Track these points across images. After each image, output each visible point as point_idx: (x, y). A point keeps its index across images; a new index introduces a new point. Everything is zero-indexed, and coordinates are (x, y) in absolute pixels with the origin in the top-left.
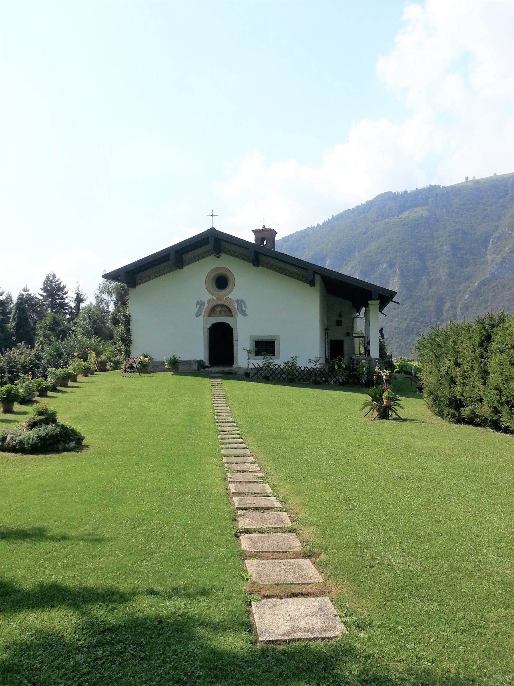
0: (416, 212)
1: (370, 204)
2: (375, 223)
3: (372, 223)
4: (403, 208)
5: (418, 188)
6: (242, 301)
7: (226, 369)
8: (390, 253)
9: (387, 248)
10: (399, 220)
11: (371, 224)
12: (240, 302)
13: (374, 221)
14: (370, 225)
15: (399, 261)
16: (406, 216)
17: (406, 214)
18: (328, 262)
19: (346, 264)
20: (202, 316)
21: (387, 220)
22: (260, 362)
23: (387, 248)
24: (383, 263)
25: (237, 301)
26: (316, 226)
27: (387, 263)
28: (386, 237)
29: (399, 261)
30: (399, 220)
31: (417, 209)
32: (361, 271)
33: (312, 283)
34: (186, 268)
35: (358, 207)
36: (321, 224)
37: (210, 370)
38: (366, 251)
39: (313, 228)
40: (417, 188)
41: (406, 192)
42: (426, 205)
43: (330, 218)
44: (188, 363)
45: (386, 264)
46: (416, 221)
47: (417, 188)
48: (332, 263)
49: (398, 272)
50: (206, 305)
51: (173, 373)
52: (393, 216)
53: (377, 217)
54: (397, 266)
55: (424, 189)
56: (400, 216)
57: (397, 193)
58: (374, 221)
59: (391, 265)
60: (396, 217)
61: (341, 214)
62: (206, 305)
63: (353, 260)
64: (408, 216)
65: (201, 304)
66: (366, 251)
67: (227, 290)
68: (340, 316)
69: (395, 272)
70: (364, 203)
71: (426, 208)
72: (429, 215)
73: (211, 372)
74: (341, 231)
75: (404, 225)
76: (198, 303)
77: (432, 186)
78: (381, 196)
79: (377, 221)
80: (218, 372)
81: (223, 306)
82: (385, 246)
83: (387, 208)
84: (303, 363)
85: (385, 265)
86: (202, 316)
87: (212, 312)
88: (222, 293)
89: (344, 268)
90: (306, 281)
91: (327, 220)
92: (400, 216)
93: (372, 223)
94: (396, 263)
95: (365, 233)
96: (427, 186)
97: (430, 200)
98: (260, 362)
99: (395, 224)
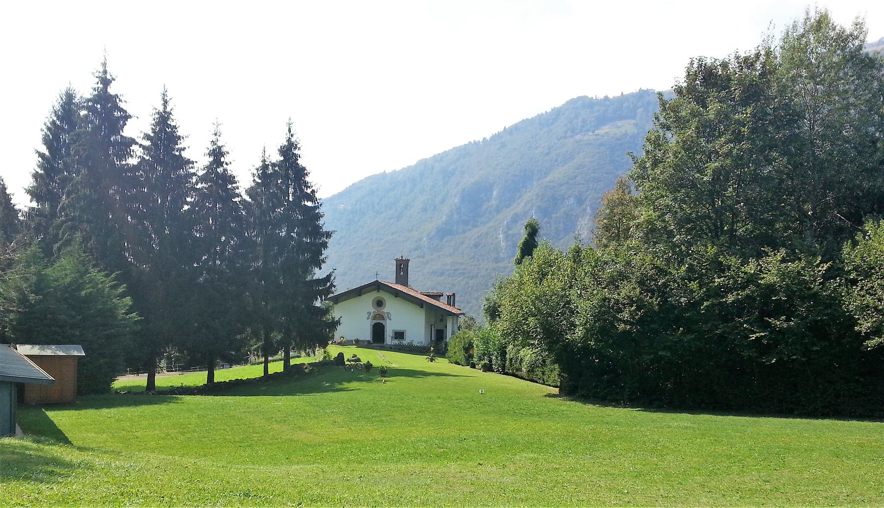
0: (618, 127)
1: (557, 113)
2: (562, 140)
3: (559, 140)
4: (602, 121)
5: (624, 93)
6: (389, 313)
7: (380, 345)
8: (580, 184)
9: (575, 177)
10: (595, 137)
11: (557, 142)
12: (388, 313)
13: (561, 138)
14: (555, 143)
15: (590, 196)
16: (605, 133)
17: (604, 130)
18: (495, 193)
19: (520, 197)
20: (370, 320)
21: (577, 137)
22: (396, 342)
23: (575, 177)
24: (570, 197)
25: (387, 313)
26: (481, 140)
27: (574, 198)
28: (575, 161)
29: (590, 196)
30: (595, 137)
31: (619, 123)
32: (539, 207)
33: (422, 307)
34: (363, 296)
35: (540, 116)
36: (488, 138)
37: (373, 345)
38: (548, 179)
39: (476, 143)
40: (622, 93)
41: (606, 98)
42: (634, 117)
43: (502, 129)
44: (363, 341)
45: (573, 199)
46: (618, 139)
47: (622, 93)
48: (501, 194)
49: (589, 210)
50: (372, 314)
51: (47, 153)
52: (588, 131)
53: (566, 132)
54: (588, 202)
55: (632, 95)
56: (597, 132)
57: (594, 98)
58: (561, 138)
59: (580, 201)
60: (590, 133)
61: (516, 124)
62: (372, 314)
63: (529, 192)
64: (607, 132)
65: (369, 313)
66: (548, 179)
67: (382, 308)
68: (442, 316)
69: (585, 210)
70: (549, 110)
71: (633, 121)
72: (636, 131)
73: (374, 346)
74: (515, 149)
75: (601, 145)
76: (368, 313)
77: (644, 91)
78: (572, 102)
79: (565, 137)
80: (378, 346)
81: (379, 315)
82: (573, 173)
83: (580, 119)
84: (415, 344)
85: (572, 200)
86: (370, 320)
87: (374, 318)
88: (379, 309)
89: (516, 203)
90: (419, 305)
91: (497, 133)
92: (597, 132)
93: (559, 140)
94: (586, 199)
95: (548, 154)
96: (636, 90)
97: (639, 111)
98: (396, 342)
99: (589, 144)
